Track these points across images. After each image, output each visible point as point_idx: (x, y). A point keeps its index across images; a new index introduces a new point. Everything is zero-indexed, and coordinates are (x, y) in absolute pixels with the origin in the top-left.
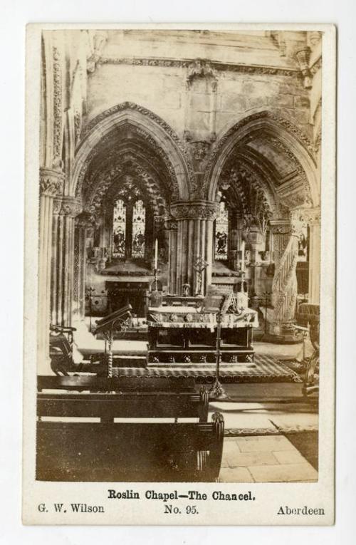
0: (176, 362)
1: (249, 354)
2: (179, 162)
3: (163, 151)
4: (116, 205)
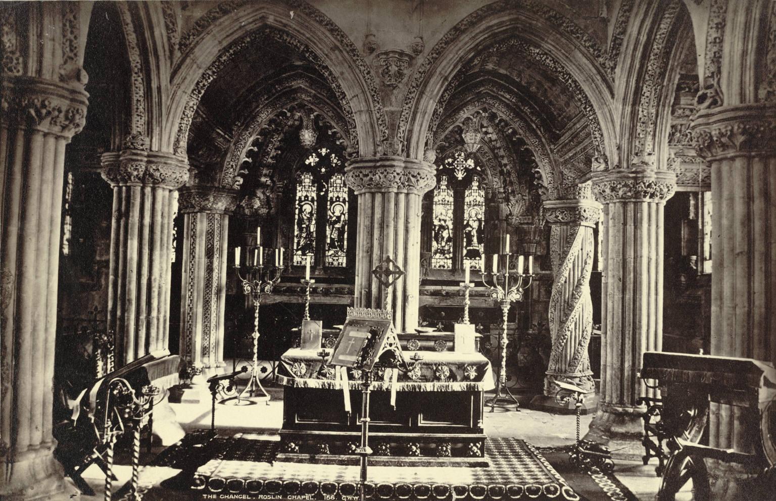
0: (332, 453)
1: (475, 441)
2: (357, 91)
3: (331, 74)
4: (301, 183)
